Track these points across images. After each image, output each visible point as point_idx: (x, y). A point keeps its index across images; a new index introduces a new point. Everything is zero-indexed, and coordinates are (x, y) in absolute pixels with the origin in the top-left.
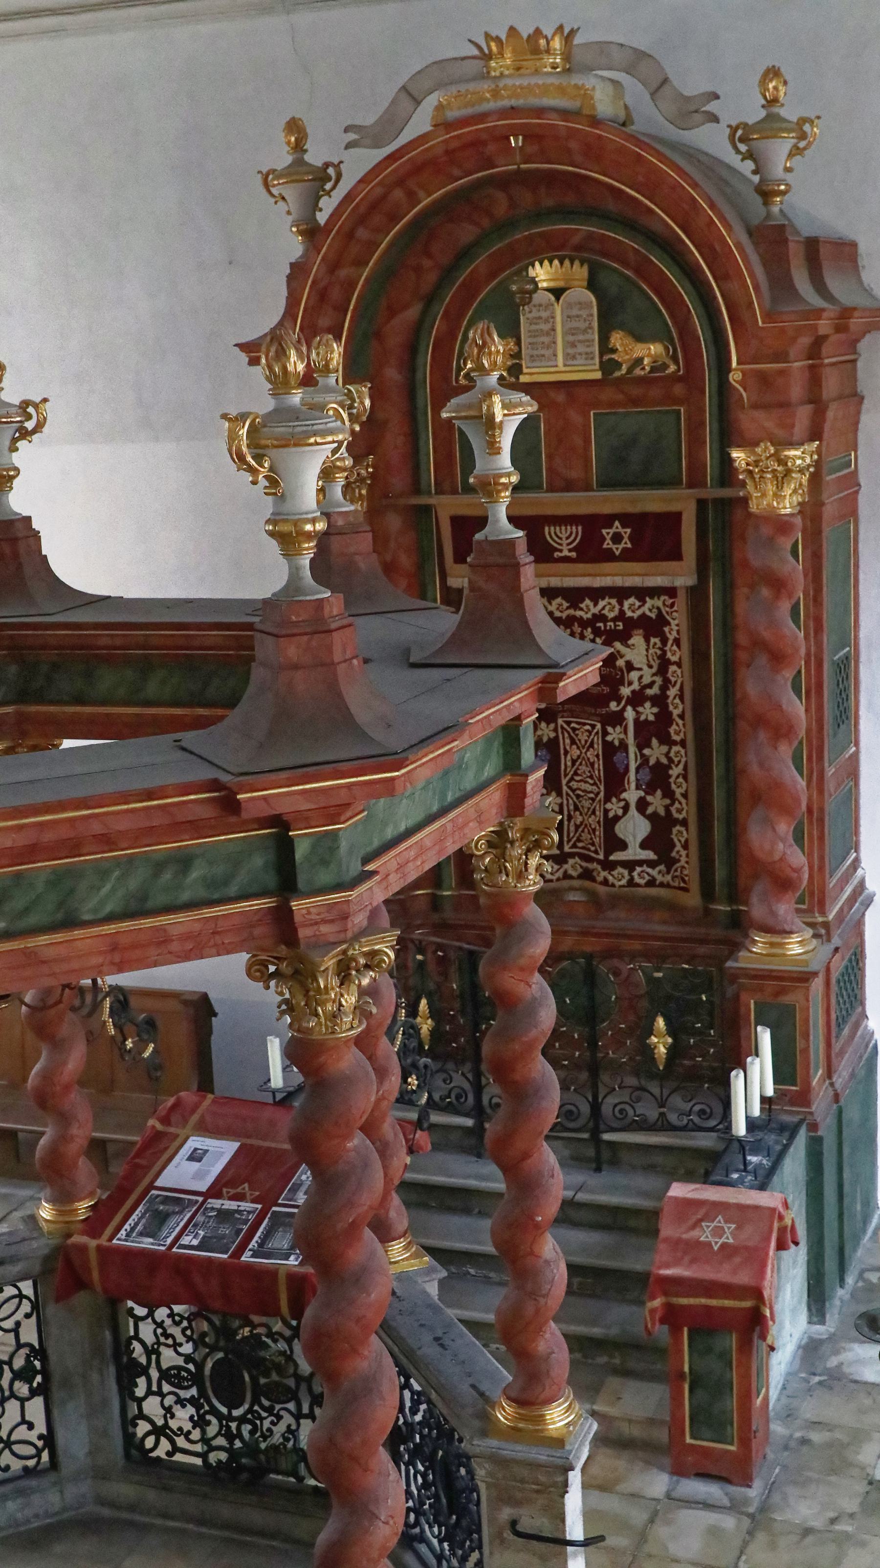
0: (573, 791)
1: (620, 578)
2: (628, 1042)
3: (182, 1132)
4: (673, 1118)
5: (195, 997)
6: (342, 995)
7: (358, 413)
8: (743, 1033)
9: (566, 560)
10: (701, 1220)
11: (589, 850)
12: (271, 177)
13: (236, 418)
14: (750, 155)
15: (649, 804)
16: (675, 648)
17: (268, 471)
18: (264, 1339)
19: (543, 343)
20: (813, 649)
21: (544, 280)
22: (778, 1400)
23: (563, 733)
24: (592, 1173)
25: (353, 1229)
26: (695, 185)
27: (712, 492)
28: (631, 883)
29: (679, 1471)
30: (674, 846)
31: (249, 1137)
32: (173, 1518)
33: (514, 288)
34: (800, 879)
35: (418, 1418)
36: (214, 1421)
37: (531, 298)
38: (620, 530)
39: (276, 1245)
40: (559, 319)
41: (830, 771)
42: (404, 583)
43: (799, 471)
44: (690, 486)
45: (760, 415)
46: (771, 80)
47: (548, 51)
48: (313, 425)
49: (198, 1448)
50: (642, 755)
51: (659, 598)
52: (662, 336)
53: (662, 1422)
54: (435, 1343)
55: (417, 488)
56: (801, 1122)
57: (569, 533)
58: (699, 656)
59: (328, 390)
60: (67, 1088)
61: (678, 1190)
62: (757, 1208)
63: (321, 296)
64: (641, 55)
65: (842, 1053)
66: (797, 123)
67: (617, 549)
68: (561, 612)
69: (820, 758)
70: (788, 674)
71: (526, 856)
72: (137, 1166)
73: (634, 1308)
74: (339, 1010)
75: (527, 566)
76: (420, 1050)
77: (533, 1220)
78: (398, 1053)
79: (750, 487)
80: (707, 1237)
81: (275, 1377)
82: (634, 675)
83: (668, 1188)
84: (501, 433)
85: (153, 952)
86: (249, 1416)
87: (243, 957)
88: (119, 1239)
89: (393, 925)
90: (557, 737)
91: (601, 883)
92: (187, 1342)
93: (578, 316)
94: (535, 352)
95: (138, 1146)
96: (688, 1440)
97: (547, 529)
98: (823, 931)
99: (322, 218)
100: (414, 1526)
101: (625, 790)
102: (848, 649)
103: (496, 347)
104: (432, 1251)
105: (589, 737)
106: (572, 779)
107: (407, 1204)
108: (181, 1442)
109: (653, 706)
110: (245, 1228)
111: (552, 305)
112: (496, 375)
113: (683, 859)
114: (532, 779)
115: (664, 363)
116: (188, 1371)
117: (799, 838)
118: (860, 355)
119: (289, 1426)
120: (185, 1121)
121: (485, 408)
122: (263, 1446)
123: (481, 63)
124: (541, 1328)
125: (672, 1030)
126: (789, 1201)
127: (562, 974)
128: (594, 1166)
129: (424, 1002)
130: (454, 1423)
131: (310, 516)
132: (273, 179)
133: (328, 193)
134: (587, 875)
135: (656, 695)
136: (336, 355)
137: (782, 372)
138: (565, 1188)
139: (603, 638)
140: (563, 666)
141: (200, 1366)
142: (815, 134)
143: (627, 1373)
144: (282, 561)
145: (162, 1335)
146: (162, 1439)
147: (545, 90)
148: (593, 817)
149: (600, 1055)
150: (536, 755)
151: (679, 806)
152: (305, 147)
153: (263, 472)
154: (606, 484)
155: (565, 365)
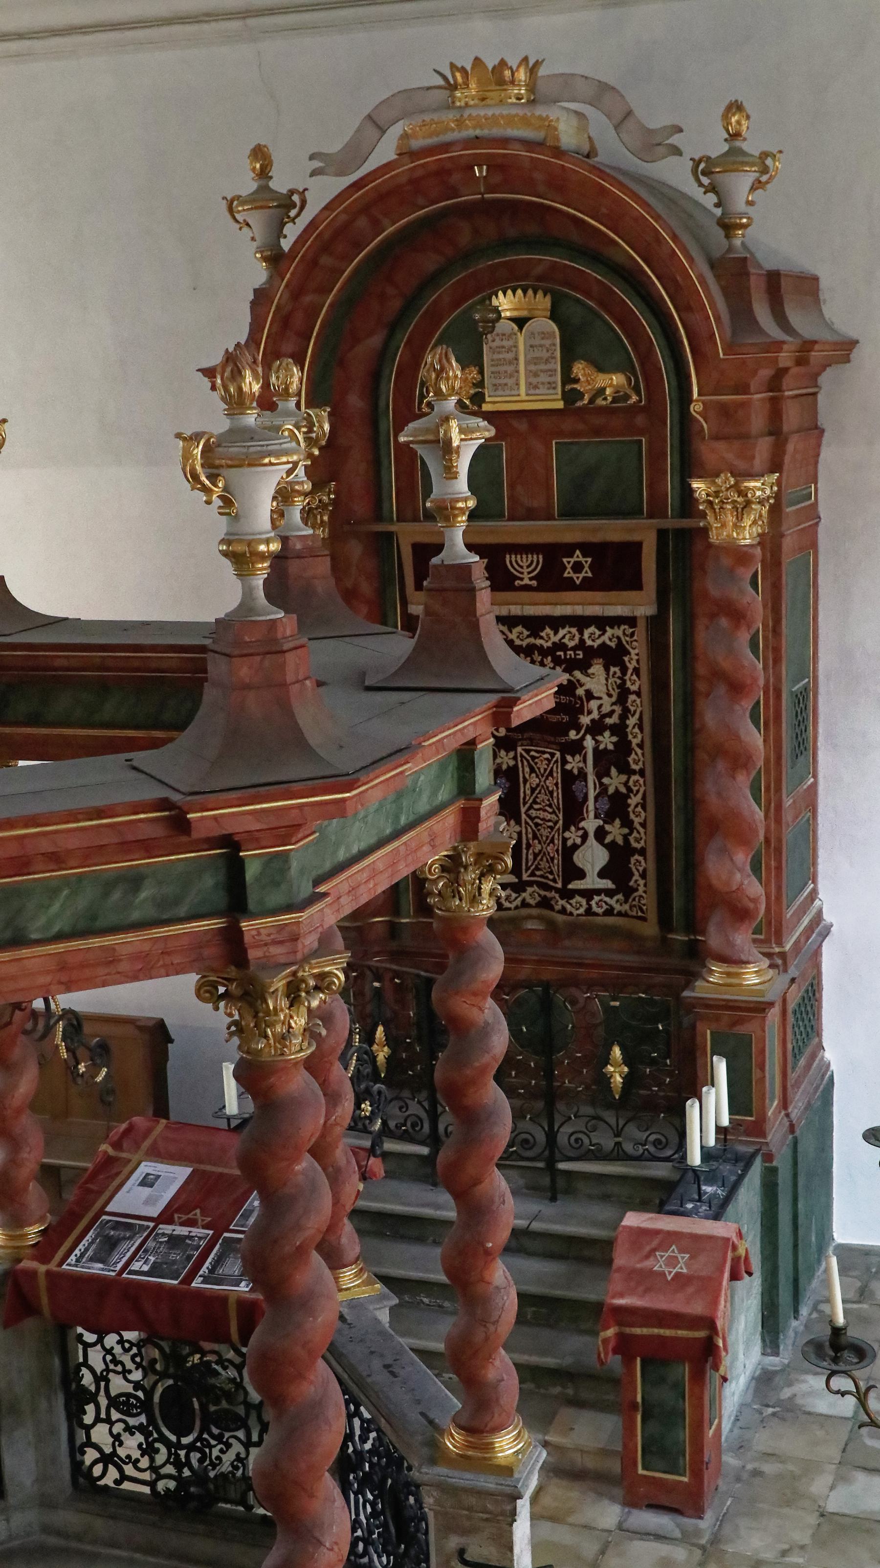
0: (532, 819)
1: (580, 607)
2: (585, 1071)
3: (135, 1158)
4: (628, 1147)
5: (151, 1024)
6: (291, 1017)
7: (317, 436)
8: (699, 1062)
9: (527, 588)
10: (654, 1250)
11: (547, 878)
12: (235, 203)
13: (191, 438)
14: (712, 189)
15: (607, 833)
16: (634, 677)
17: (222, 491)
18: (214, 1366)
19: (506, 372)
20: (771, 680)
21: (507, 310)
22: (731, 1431)
23: (522, 761)
24: (547, 1202)
25: (301, 1252)
26: (658, 218)
27: (671, 523)
28: (589, 912)
29: (632, 1502)
30: (633, 875)
31: (200, 1162)
32: (118, 1547)
33: (477, 316)
34: (757, 909)
35: (368, 1446)
36: (163, 1450)
37: (494, 327)
38: (581, 559)
39: (227, 1272)
40: (521, 347)
41: (788, 802)
42: (365, 610)
43: (759, 503)
44: (651, 516)
45: (721, 446)
46: (734, 115)
47: (512, 82)
48: (267, 445)
49: (147, 1476)
50: (601, 784)
51: (619, 628)
52: (626, 367)
53: (613, 1453)
54: (385, 1371)
55: (379, 515)
56: (757, 1152)
57: (529, 562)
58: (659, 685)
59: (288, 414)
60: (19, 1111)
61: (632, 1219)
62: (711, 1238)
63: (284, 322)
64: (604, 88)
65: (797, 1084)
66: (760, 158)
67: (578, 578)
68: (522, 640)
69: (778, 789)
70: (747, 704)
71: (480, 879)
72: (90, 1191)
73: (587, 1339)
74: (289, 1032)
75: (483, 591)
76: (375, 1076)
77: (483, 1246)
78: (351, 1079)
79: (710, 517)
80: (661, 1266)
81: (224, 1404)
82: (594, 704)
83: (621, 1219)
84: (458, 457)
85: (101, 971)
86: (199, 1444)
87: (192, 979)
88: (69, 1265)
89: (347, 948)
90: (516, 766)
91: (559, 912)
92: (137, 1369)
93: (541, 346)
94: (498, 381)
95: (89, 1172)
96: (640, 1471)
97: (508, 556)
98: (779, 962)
99: (286, 245)
100: (362, 1556)
101: (584, 819)
102: (807, 680)
103: (454, 372)
104: (386, 1280)
105: (548, 765)
106: (531, 808)
107: (359, 1231)
108: (129, 1470)
109: (612, 735)
110: (196, 1254)
111: (515, 334)
112: (454, 399)
113: (641, 889)
114: (486, 803)
115: (626, 394)
116: (137, 1398)
117: (756, 868)
118: (820, 388)
119: (238, 1455)
120: (137, 1146)
121: (442, 432)
122: (212, 1474)
123: (448, 92)
124: (490, 1357)
125: (627, 1060)
126: (744, 1231)
127: (518, 1003)
128: (549, 1194)
129: (380, 1029)
130: (403, 1451)
131: (264, 536)
132: (237, 206)
133: (293, 220)
134: (545, 903)
135: (615, 724)
136: (296, 380)
137: (743, 405)
138: (516, 1218)
139: (563, 666)
140: (518, 691)
141: (149, 1394)
142: (777, 168)
143: (578, 1403)
144: (238, 584)
145: (111, 1361)
146: (111, 1467)
147: (510, 120)
148: (551, 845)
149: (557, 1084)
150: (496, 783)
151: (638, 836)
152: (270, 174)
153: (217, 491)
154: (568, 513)
155: (527, 395)
